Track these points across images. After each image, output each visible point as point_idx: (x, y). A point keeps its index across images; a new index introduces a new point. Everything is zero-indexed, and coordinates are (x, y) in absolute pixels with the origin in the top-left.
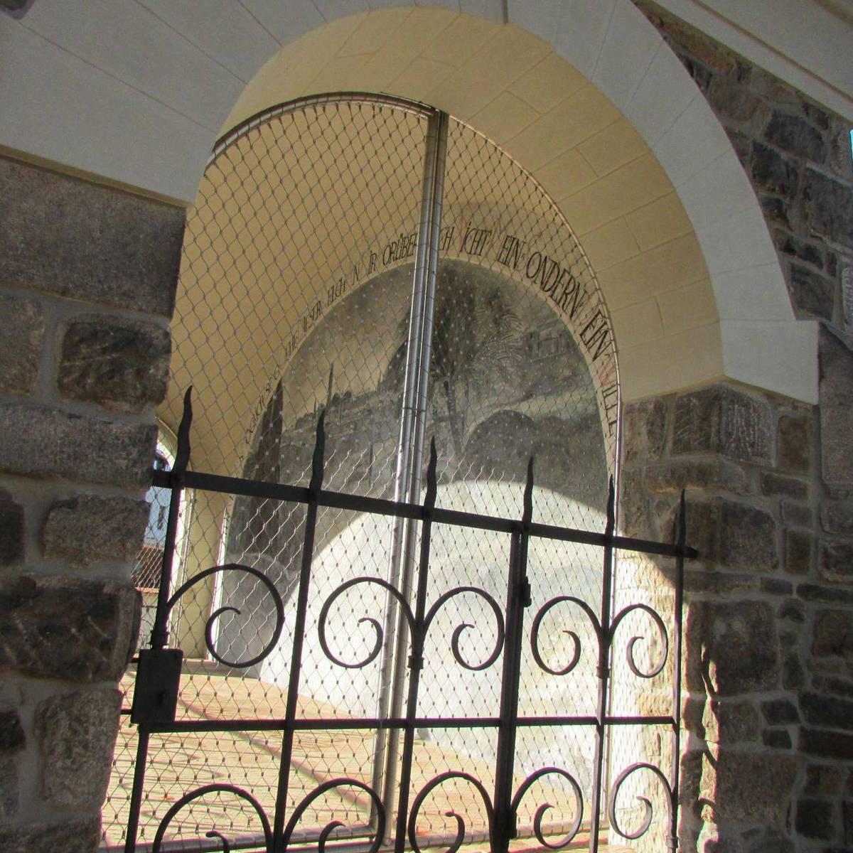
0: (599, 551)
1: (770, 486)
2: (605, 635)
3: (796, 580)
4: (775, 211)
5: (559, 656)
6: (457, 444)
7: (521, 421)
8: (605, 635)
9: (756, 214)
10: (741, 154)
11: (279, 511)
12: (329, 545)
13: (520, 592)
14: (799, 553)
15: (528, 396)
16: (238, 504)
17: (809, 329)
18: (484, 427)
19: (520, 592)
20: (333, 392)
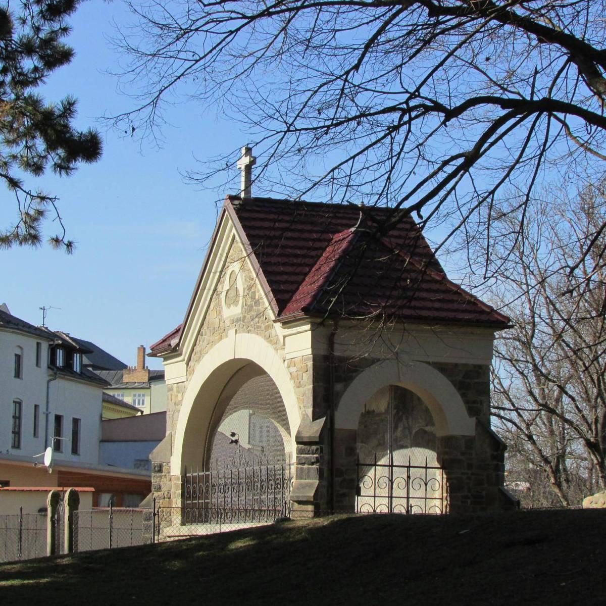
0: (424, 469)
1: (463, 454)
2: (426, 484)
3: (470, 472)
4: (463, 395)
5: (416, 487)
6: (410, 436)
7: (425, 432)
8: (426, 484)
9: (459, 397)
10: (455, 386)
11: (282, 431)
12: (249, 243)
13: (409, 477)
14: (470, 466)
15: (427, 426)
16: (109, 387)
17: (474, 420)
18: (416, 432)
19: (409, 477)
20: (367, 408)
